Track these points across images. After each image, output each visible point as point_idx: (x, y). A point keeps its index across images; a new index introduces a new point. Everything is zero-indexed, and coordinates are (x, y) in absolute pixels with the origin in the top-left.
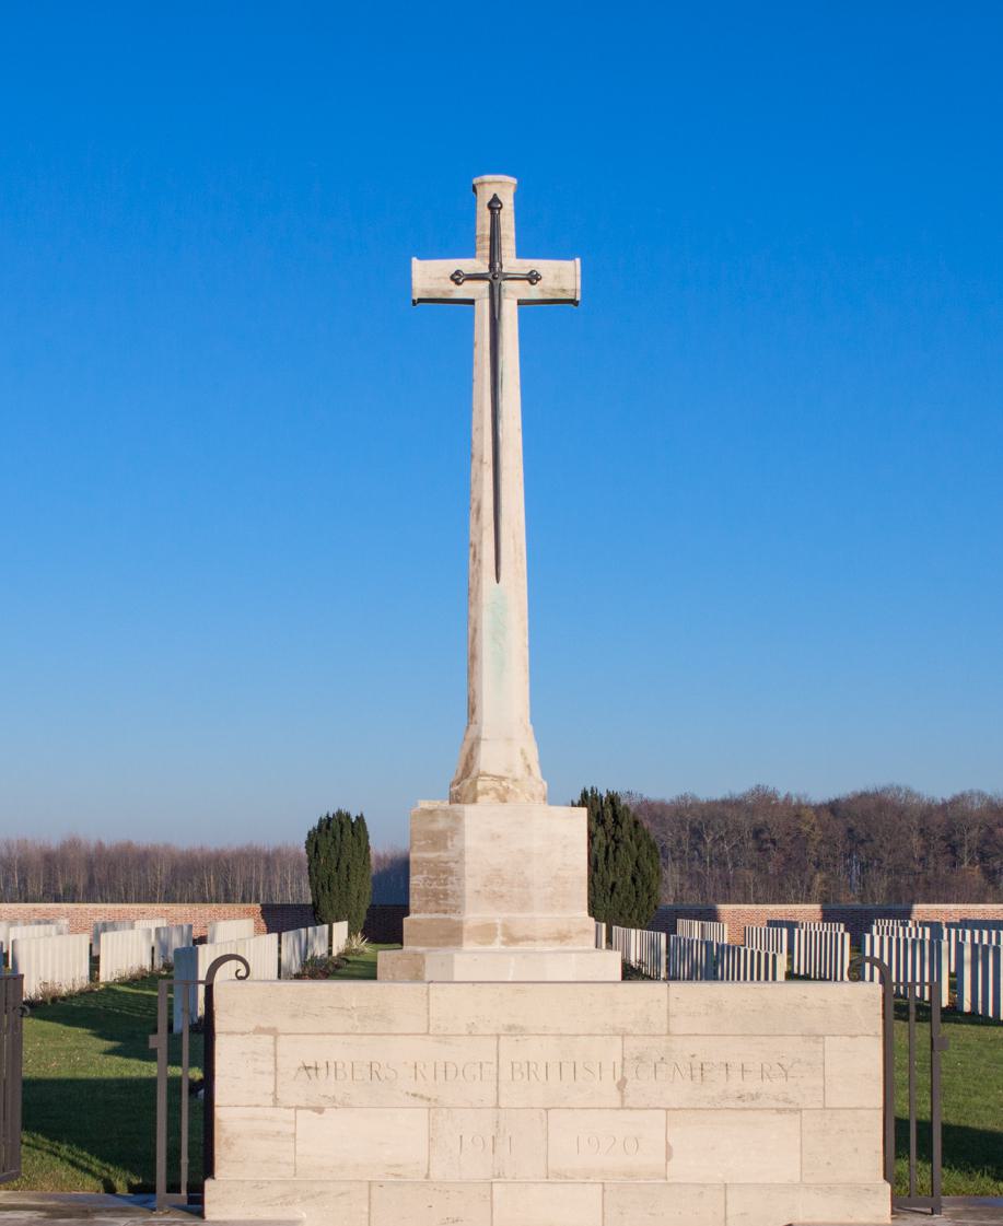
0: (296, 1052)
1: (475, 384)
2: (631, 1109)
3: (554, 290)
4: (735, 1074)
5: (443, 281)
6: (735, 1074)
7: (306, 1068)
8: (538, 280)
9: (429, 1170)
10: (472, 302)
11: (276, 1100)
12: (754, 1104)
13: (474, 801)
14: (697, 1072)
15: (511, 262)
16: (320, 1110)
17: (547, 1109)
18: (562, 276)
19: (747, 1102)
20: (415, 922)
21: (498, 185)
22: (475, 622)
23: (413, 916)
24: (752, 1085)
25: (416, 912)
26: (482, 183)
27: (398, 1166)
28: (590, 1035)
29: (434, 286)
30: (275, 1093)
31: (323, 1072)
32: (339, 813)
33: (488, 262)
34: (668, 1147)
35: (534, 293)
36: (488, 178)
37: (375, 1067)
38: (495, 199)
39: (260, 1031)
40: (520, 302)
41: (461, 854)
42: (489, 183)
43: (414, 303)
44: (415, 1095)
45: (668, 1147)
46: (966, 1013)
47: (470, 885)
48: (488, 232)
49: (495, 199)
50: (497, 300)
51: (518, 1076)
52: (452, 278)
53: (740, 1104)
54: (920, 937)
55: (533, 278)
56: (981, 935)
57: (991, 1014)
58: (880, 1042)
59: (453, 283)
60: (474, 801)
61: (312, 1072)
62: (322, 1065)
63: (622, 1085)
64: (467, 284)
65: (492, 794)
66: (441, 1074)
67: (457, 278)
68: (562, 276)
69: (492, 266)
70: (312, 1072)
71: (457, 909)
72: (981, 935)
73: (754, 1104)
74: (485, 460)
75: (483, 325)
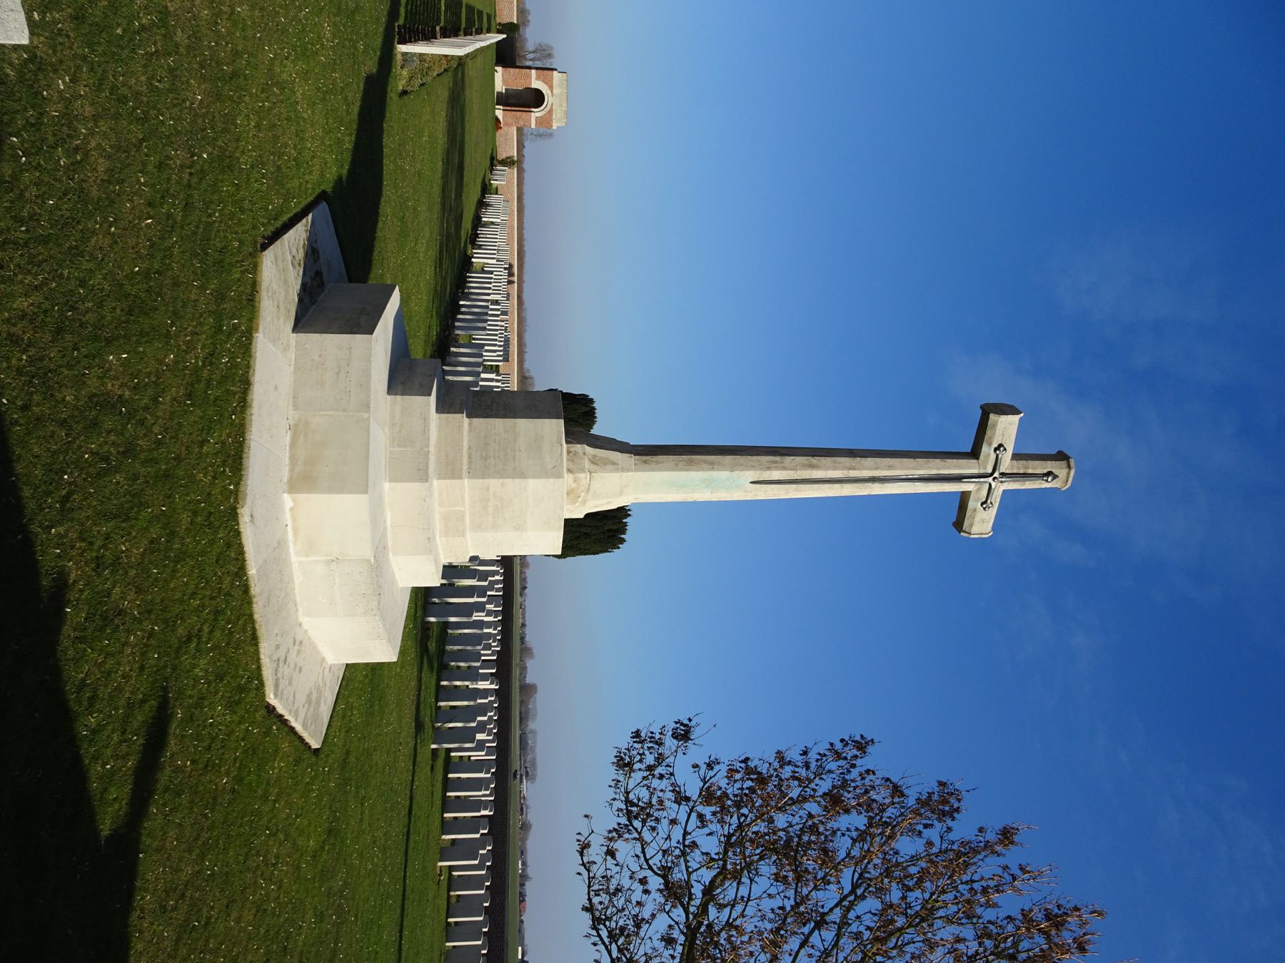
1: (912, 460)
3: (974, 518)
5: (1000, 438)
8: (984, 509)
15: (1000, 488)
20: (460, 428)
21: (1064, 479)
22: (719, 464)
23: (466, 421)
25: (470, 424)
26: (1069, 467)
29: (997, 431)
32: (529, 21)
33: (1008, 472)
35: (973, 504)
36: (1073, 472)
38: (1055, 477)
41: (523, 476)
42: (1069, 474)
46: (444, 648)
47: (494, 483)
48: (1030, 471)
49: (1055, 477)
50: (976, 480)
52: (1001, 445)
54: (490, 312)
57: (460, 316)
59: (996, 446)
64: (993, 456)
65: (574, 485)
68: (982, 523)
71: (473, 474)
72: (500, 346)
74: (851, 471)
75: (960, 468)
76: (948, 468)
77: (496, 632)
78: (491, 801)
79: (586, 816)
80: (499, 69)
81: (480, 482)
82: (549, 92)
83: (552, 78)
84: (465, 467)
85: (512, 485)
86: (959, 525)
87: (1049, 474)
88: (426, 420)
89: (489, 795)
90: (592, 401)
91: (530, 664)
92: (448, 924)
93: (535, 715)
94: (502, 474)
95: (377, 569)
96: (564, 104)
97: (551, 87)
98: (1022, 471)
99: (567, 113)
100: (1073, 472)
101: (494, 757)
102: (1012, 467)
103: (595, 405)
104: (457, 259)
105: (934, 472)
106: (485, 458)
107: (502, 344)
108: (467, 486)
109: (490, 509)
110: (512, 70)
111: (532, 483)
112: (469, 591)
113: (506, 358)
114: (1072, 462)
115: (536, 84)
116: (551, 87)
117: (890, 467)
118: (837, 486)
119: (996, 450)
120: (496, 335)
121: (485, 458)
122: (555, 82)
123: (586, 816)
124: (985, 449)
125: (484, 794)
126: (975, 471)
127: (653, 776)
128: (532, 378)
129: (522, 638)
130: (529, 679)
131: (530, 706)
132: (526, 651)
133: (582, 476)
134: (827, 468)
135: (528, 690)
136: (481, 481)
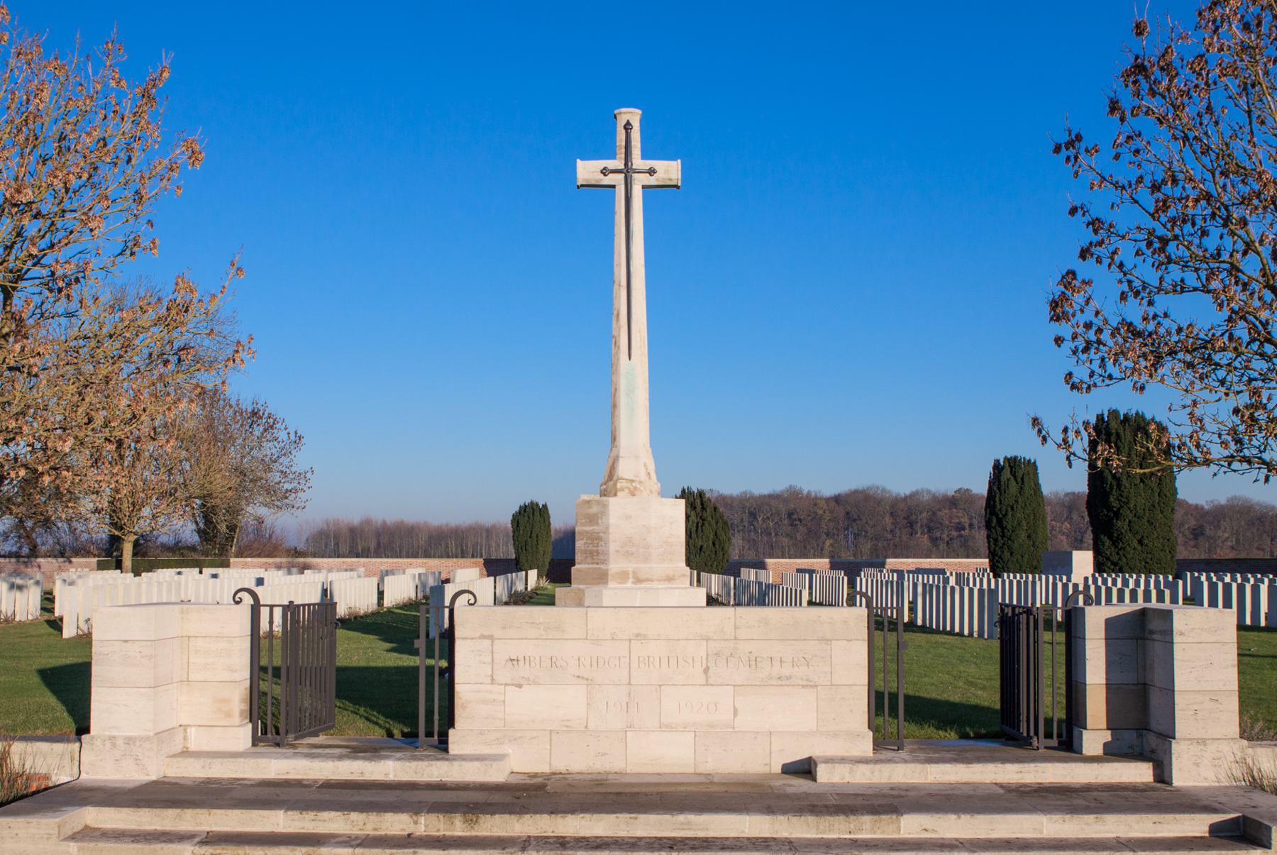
0: (505, 650)
2: (712, 685)
4: (777, 664)
6: (777, 664)
10: (614, 187)
11: (493, 680)
12: (788, 682)
13: (615, 495)
14: (753, 663)
15: (638, 162)
16: (520, 686)
17: (660, 686)
18: (669, 170)
19: (783, 681)
20: (579, 570)
23: (577, 566)
24: (787, 671)
25: (579, 564)
26: (620, 113)
28: (126, 641)
30: (492, 676)
31: (521, 663)
35: (652, 181)
36: (623, 110)
37: (554, 660)
38: (628, 123)
39: (483, 637)
40: (644, 187)
42: (625, 113)
43: (578, 187)
44: (578, 677)
48: (624, 144)
49: (628, 123)
53: (780, 682)
55: (651, 172)
57: (934, 627)
61: (515, 662)
62: (521, 658)
63: (706, 670)
64: (611, 176)
65: (627, 491)
66: (594, 664)
67: (605, 172)
68: (669, 170)
69: (626, 164)
70: (515, 662)
71: (605, 562)
73: (788, 682)
76: (621, 192)
86: (676, 186)
95: (686, 588)
98: (624, 150)
102: (621, 158)
104: (666, 586)
111: (612, 521)
112: (1098, 589)
117: (620, 255)
118: (633, 263)
119: (605, 175)
127: (1139, 357)
136: (611, 556)
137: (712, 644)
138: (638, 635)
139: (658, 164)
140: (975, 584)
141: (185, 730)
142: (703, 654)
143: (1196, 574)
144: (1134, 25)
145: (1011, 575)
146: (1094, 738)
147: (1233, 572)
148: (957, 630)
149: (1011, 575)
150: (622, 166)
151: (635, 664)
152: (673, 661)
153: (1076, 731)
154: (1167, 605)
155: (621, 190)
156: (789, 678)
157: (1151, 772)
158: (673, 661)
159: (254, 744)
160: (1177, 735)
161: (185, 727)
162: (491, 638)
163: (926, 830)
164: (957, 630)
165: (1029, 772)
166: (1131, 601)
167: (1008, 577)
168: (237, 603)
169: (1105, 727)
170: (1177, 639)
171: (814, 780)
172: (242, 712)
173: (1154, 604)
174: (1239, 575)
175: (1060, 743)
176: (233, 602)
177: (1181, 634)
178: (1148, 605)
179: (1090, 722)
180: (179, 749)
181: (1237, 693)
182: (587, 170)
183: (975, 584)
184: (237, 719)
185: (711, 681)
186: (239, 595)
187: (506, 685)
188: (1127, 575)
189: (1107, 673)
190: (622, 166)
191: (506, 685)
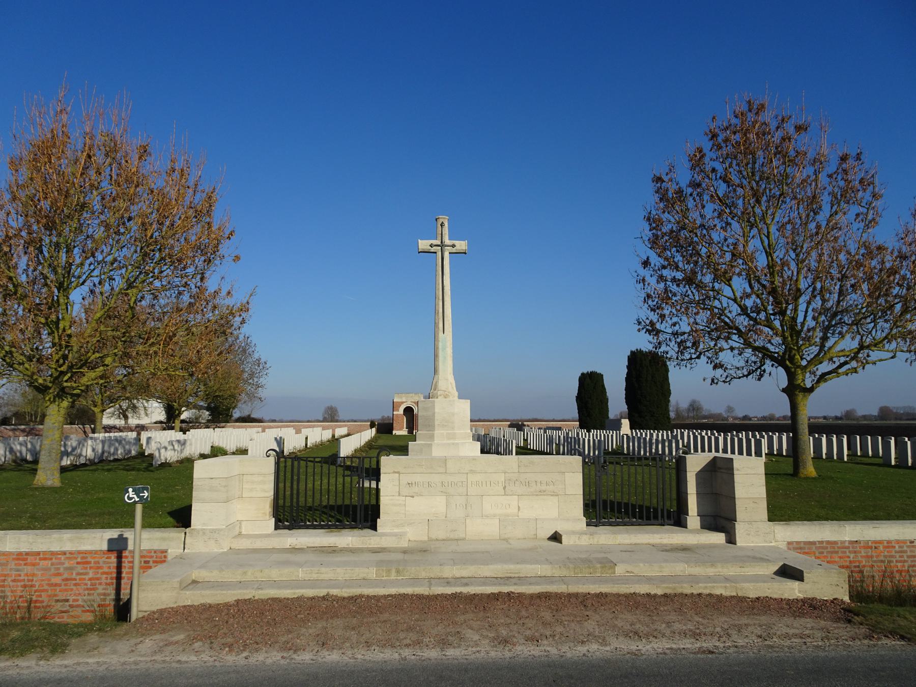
0: (405, 479)
4: (539, 484)
6: (539, 484)
7: (409, 484)
9: (190, 584)
10: (436, 253)
11: (399, 494)
12: (545, 493)
13: (437, 398)
14: (527, 484)
16: (413, 497)
18: (461, 245)
19: (542, 493)
20: (420, 434)
24: (544, 487)
27: (437, 514)
31: (414, 485)
34: (519, 507)
35: (454, 250)
36: (440, 217)
37: (430, 483)
38: (443, 223)
39: (396, 472)
40: (450, 253)
41: (434, 413)
43: (419, 252)
45: (519, 507)
47: (436, 423)
49: (443, 223)
51: (473, 485)
53: (540, 493)
55: (453, 246)
56: (597, 432)
58: (581, 474)
60: (437, 398)
62: (414, 483)
63: (504, 488)
64: (434, 248)
65: (442, 396)
66: (450, 485)
67: (431, 246)
68: (461, 245)
69: (442, 242)
72: (597, 432)
73: (545, 493)
77: (766, 436)
78: (837, 437)
79: (704, 380)
80: (394, 432)
81: (436, 427)
82: (405, 404)
83: (398, 402)
84: (431, 432)
85: (437, 417)
87: (441, 226)
88: (419, 444)
89: (775, 434)
90: (583, 374)
91: (860, 412)
92: (826, 458)
93: (910, 407)
94: (434, 420)
96: (411, 395)
97: (402, 403)
99: (416, 394)
100: (440, 217)
101: (858, 437)
103: (585, 372)
105: (440, 268)
106: (429, 426)
107: (611, 432)
108: (437, 432)
109: (446, 424)
110: (394, 425)
111: (436, 410)
113: (559, 429)
114: (437, 217)
115: (401, 411)
116: (402, 403)
118: (445, 303)
120: (608, 435)
121: (429, 426)
122: (399, 400)
123: (704, 380)
124: (432, 251)
125: (743, 435)
126: (440, 253)
128: (621, 413)
129: (837, 418)
130: (875, 412)
131: (902, 412)
132: (849, 415)
133: (439, 393)
134: (439, 308)
135: (885, 412)
137: (507, 475)
138: (471, 470)
139: (456, 243)
140: (586, 437)
141: (240, 523)
142: (503, 479)
143: (683, 430)
144: (8, 160)
145: (605, 431)
146: (693, 519)
147: (707, 430)
148: (532, 448)
149: (605, 431)
150: (439, 243)
151: (469, 485)
152: (488, 483)
153: (682, 516)
154: (729, 455)
155: (439, 254)
156: (544, 491)
157: (724, 538)
158: (488, 483)
159: (276, 529)
160: (738, 520)
161: (240, 522)
162: (398, 473)
163: (628, 572)
164: (532, 448)
165: (665, 538)
166: (708, 452)
167: (603, 433)
168: (268, 456)
169: (696, 514)
170: (735, 472)
171: (561, 543)
172: (270, 513)
173: (721, 454)
174: (709, 431)
175: (674, 522)
176: (265, 456)
177: (738, 470)
178: (717, 455)
179: (690, 513)
180: (237, 533)
181: (766, 499)
182: (424, 244)
183: (586, 437)
184: (268, 517)
185: (369, 459)
186: (269, 452)
187: (406, 496)
188: (652, 431)
189: (697, 488)
190: (439, 243)
191: (406, 496)
